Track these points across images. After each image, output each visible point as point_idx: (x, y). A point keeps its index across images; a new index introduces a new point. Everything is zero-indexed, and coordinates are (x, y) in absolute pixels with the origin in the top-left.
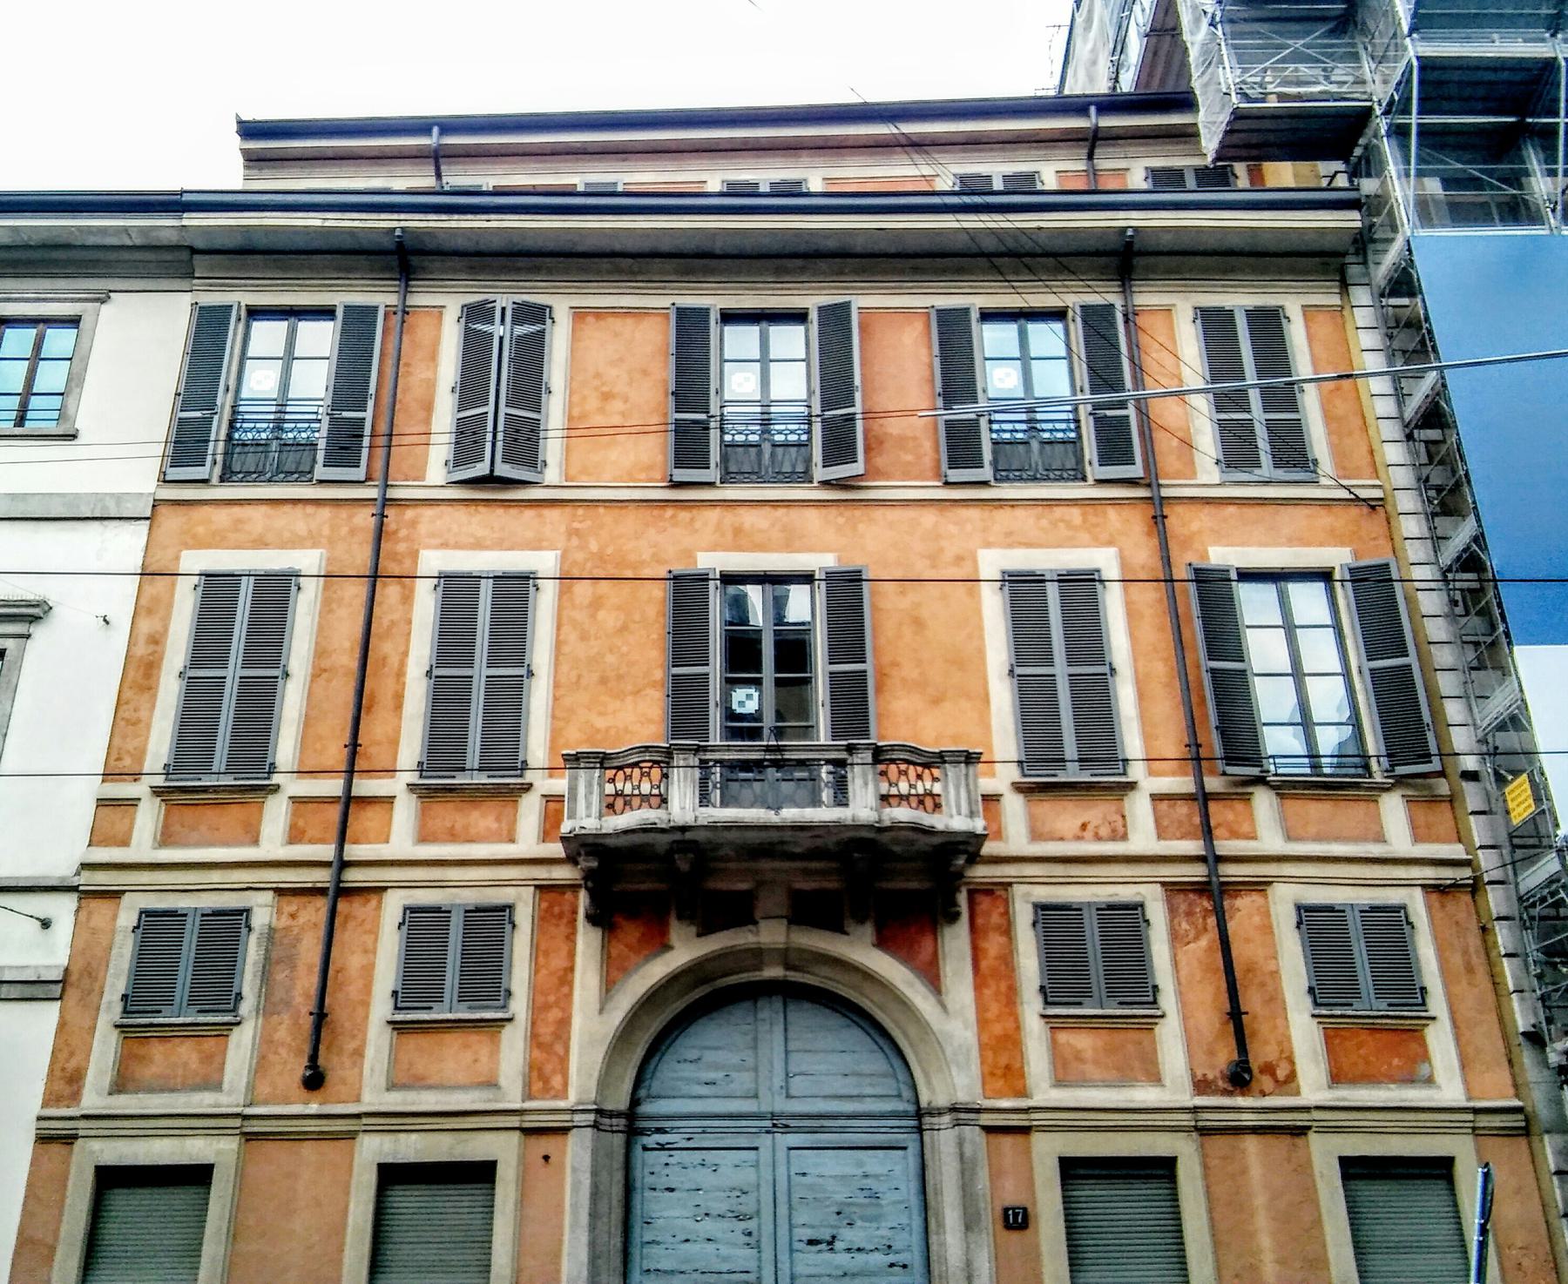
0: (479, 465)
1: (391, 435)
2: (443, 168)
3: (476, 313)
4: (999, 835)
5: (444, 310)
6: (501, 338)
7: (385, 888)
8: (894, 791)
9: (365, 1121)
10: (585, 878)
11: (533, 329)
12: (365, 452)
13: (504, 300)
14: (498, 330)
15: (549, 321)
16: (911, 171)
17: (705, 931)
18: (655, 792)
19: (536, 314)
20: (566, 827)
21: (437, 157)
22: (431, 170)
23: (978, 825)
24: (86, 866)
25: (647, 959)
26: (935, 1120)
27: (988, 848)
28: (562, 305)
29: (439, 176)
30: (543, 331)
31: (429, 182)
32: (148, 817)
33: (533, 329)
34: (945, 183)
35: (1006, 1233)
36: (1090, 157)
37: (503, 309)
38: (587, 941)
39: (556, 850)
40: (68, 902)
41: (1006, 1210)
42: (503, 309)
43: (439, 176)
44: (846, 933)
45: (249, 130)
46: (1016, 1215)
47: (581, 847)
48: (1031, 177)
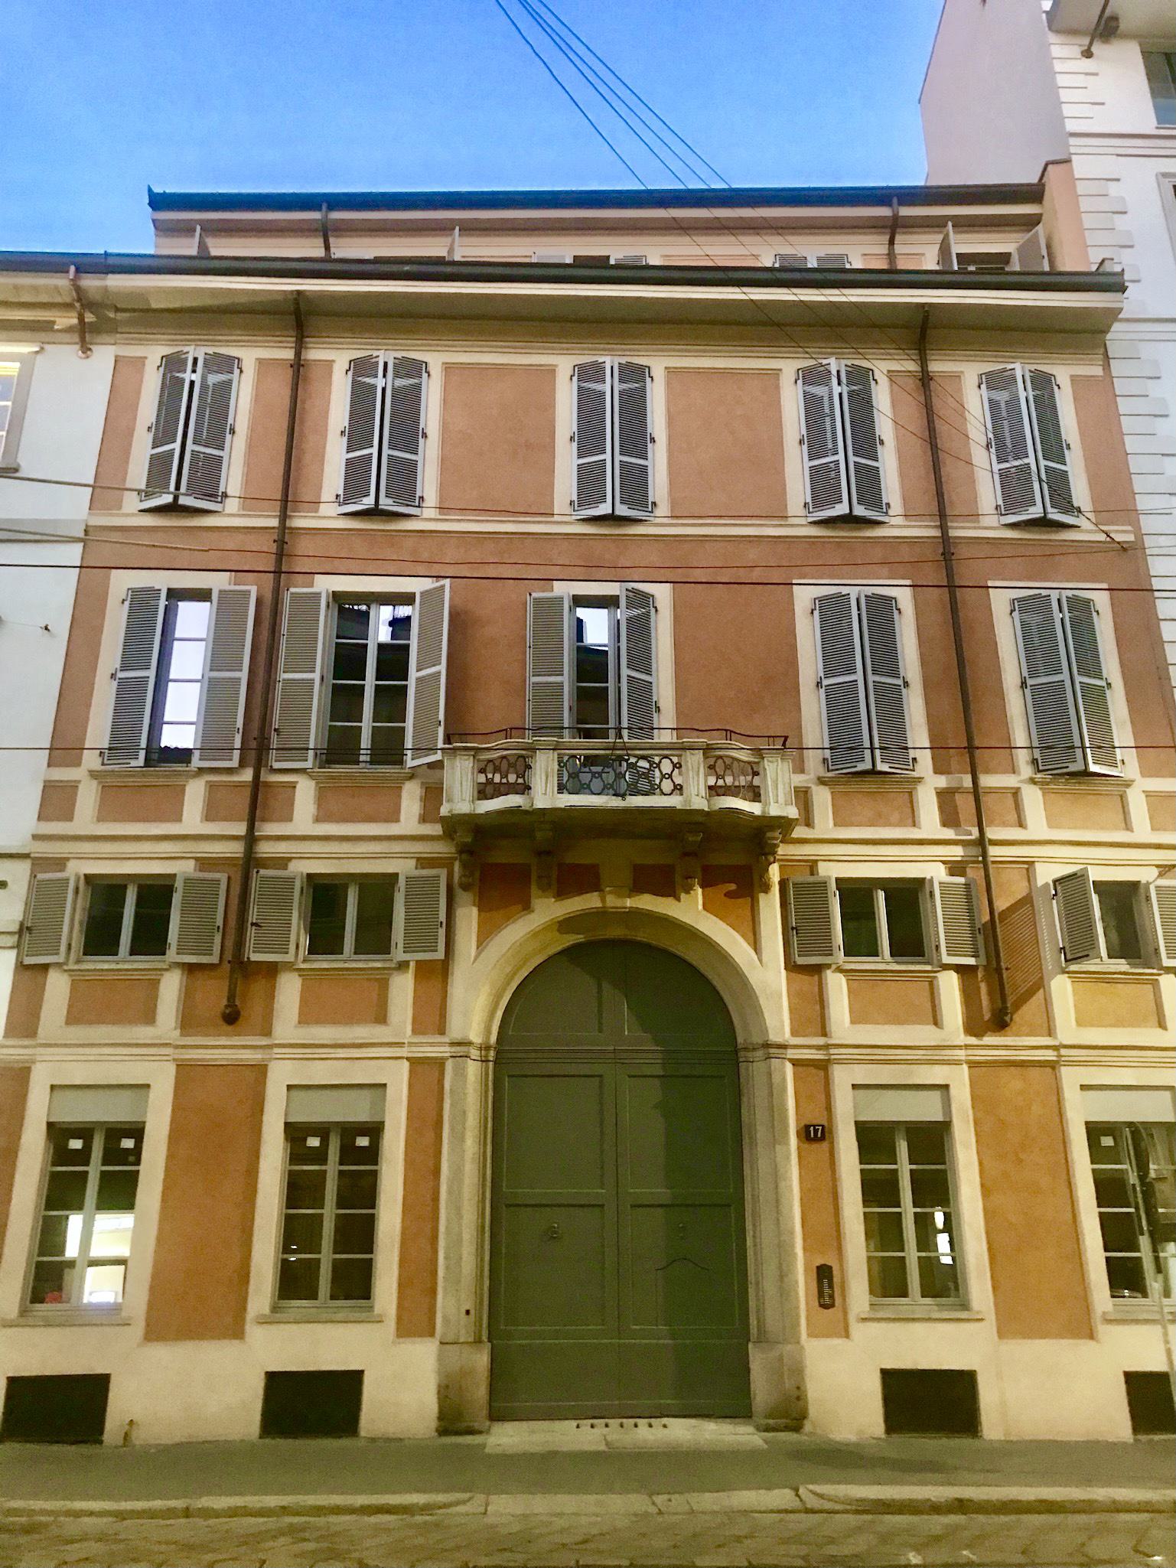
0: (602, 506)
1: (278, 573)
2: (332, 240)
3: (361, 368)
4: (809, 823)
5: (335, 358)
6: (384, 390)
7: (290, 859)
8: (720, 782)
9: (276, 1050)
10: (461, 852)
11: (412, 381)
12: (529, 634)
13: (386, 355)
14: (380, 382)
15: (425, 375)
16: (739, 250)
17: (561, 894)
18: (520, 781)
19: (413, 369)
20: (444, 811)
21: (325, 231)
22: (320, 241)
23: (793, 812)
24: (35, 837)
25: (508, 919)
26: (750, 1054)
27: (799, 832)
28: (436, 359)
29: (327, 248)
30: (418, 387)
31: (320, 253)
32: (88, 797)
33: (412, 381)
34: (767, 262)
35: (806, 1146)
36: (892, 242)
37: (386, 364)
38: (468, 917)
39: (436, 829)
40: (23, 868)
41: (807, 1127)
42: (386, 364)
43: (327, 248)
44: (679, 900)
45: (158, 202)
46: (816, 1131)
47: (453, 825)
48: (841, 257)
